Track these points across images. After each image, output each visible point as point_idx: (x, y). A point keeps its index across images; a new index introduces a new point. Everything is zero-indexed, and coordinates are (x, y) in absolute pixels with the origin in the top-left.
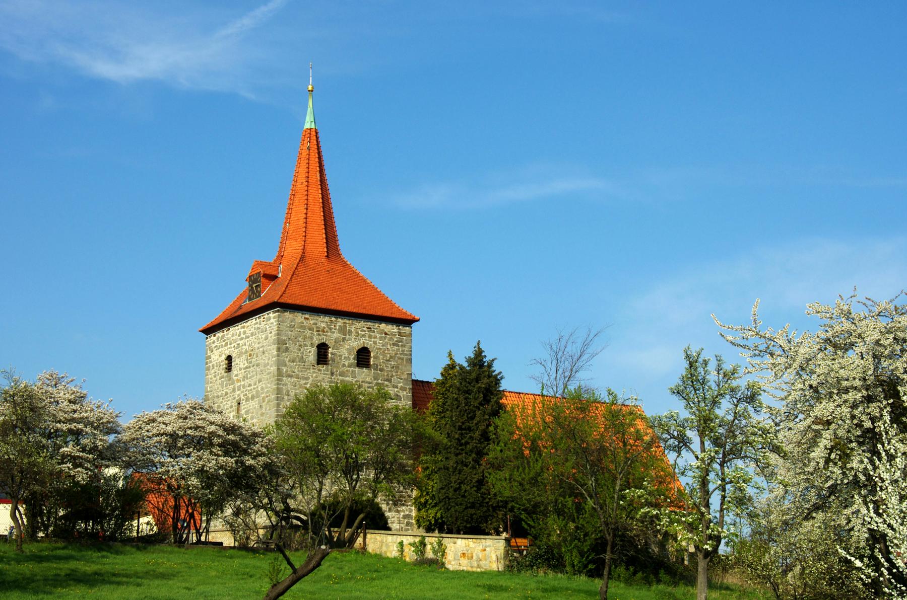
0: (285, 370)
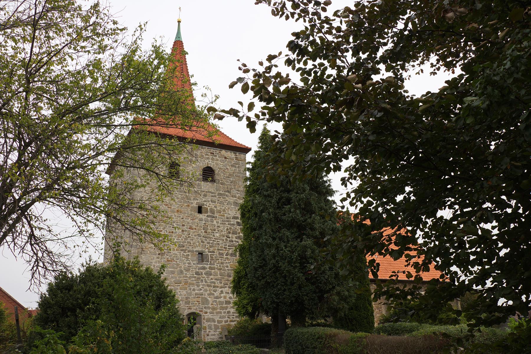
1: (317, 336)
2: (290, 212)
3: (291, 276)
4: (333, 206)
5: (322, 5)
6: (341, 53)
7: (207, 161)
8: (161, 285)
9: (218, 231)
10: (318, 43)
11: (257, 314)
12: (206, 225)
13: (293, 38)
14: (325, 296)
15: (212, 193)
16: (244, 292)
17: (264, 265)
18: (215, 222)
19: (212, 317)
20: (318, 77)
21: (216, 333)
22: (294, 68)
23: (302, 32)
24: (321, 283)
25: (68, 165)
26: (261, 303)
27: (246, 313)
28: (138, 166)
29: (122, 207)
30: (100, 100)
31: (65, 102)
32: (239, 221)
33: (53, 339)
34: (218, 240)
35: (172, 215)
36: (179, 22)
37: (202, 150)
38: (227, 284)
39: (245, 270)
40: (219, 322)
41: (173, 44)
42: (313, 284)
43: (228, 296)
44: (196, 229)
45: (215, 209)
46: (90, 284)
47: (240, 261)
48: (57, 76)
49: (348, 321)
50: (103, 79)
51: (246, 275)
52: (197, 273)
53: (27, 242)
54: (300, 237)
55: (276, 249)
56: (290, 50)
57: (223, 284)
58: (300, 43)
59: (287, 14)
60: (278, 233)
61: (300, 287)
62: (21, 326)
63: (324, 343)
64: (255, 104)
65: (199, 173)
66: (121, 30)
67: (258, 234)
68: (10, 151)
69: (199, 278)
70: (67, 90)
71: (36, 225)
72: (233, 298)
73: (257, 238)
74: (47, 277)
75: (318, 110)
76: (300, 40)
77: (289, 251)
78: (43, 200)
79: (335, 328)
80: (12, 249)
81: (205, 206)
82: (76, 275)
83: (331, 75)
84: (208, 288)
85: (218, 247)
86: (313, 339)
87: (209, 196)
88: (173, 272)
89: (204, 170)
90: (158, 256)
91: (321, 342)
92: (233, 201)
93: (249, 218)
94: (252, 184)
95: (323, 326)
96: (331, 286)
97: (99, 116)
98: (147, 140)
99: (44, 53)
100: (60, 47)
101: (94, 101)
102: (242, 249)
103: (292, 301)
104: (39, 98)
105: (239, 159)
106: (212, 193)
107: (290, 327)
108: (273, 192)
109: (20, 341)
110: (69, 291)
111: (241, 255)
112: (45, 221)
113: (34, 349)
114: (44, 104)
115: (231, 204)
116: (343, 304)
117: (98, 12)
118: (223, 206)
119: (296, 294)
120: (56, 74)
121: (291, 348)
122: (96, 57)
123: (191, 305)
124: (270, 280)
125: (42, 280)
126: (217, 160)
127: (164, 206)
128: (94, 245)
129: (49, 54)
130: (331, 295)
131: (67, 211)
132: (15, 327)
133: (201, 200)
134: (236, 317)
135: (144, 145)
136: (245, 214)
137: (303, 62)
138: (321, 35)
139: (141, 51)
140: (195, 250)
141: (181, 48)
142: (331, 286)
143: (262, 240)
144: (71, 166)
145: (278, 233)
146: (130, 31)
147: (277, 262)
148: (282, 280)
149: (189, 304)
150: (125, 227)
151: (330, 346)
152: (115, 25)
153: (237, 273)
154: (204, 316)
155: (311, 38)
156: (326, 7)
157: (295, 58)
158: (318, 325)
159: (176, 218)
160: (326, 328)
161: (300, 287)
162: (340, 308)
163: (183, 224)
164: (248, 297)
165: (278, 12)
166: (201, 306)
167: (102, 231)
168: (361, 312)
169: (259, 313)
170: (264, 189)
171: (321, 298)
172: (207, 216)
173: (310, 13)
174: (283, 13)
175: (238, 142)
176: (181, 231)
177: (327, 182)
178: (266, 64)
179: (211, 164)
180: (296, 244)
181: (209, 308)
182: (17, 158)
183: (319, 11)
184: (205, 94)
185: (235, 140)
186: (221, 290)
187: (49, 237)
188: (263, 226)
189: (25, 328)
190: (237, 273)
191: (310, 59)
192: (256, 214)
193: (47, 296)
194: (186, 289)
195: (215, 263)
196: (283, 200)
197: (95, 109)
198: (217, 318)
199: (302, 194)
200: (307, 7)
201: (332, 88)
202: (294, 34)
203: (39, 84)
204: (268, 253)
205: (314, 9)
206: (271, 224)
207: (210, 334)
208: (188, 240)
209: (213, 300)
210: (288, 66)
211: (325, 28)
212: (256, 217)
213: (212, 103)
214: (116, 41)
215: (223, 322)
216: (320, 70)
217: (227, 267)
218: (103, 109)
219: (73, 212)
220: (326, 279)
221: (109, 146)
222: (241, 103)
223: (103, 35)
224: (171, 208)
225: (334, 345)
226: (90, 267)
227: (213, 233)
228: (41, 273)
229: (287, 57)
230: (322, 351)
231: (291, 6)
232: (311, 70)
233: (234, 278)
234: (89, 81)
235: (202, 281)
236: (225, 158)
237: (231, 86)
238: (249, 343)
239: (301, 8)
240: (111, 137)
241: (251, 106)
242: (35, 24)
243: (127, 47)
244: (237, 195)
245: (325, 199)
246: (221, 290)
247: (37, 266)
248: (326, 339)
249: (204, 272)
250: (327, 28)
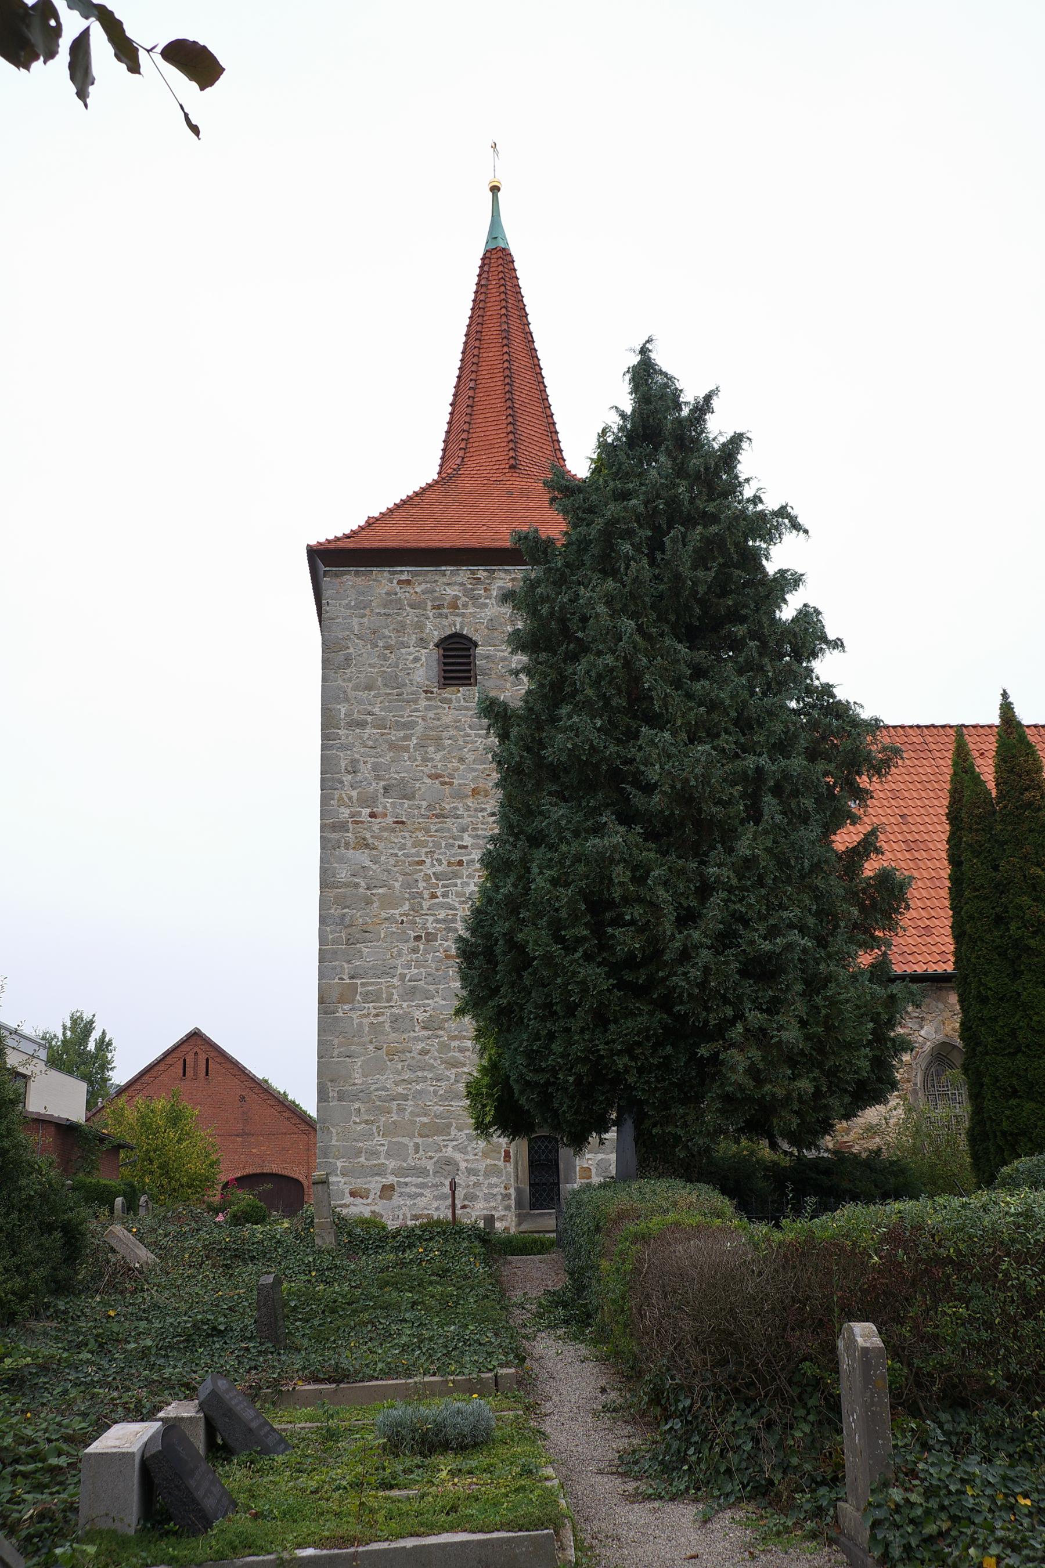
0: (343, 710)
35: (456, 808)
36: (495, 189)
90: (412, 944)
127: (428, 781)
159: (470, 816)
161: (601, 1019)
224: (451, 784)
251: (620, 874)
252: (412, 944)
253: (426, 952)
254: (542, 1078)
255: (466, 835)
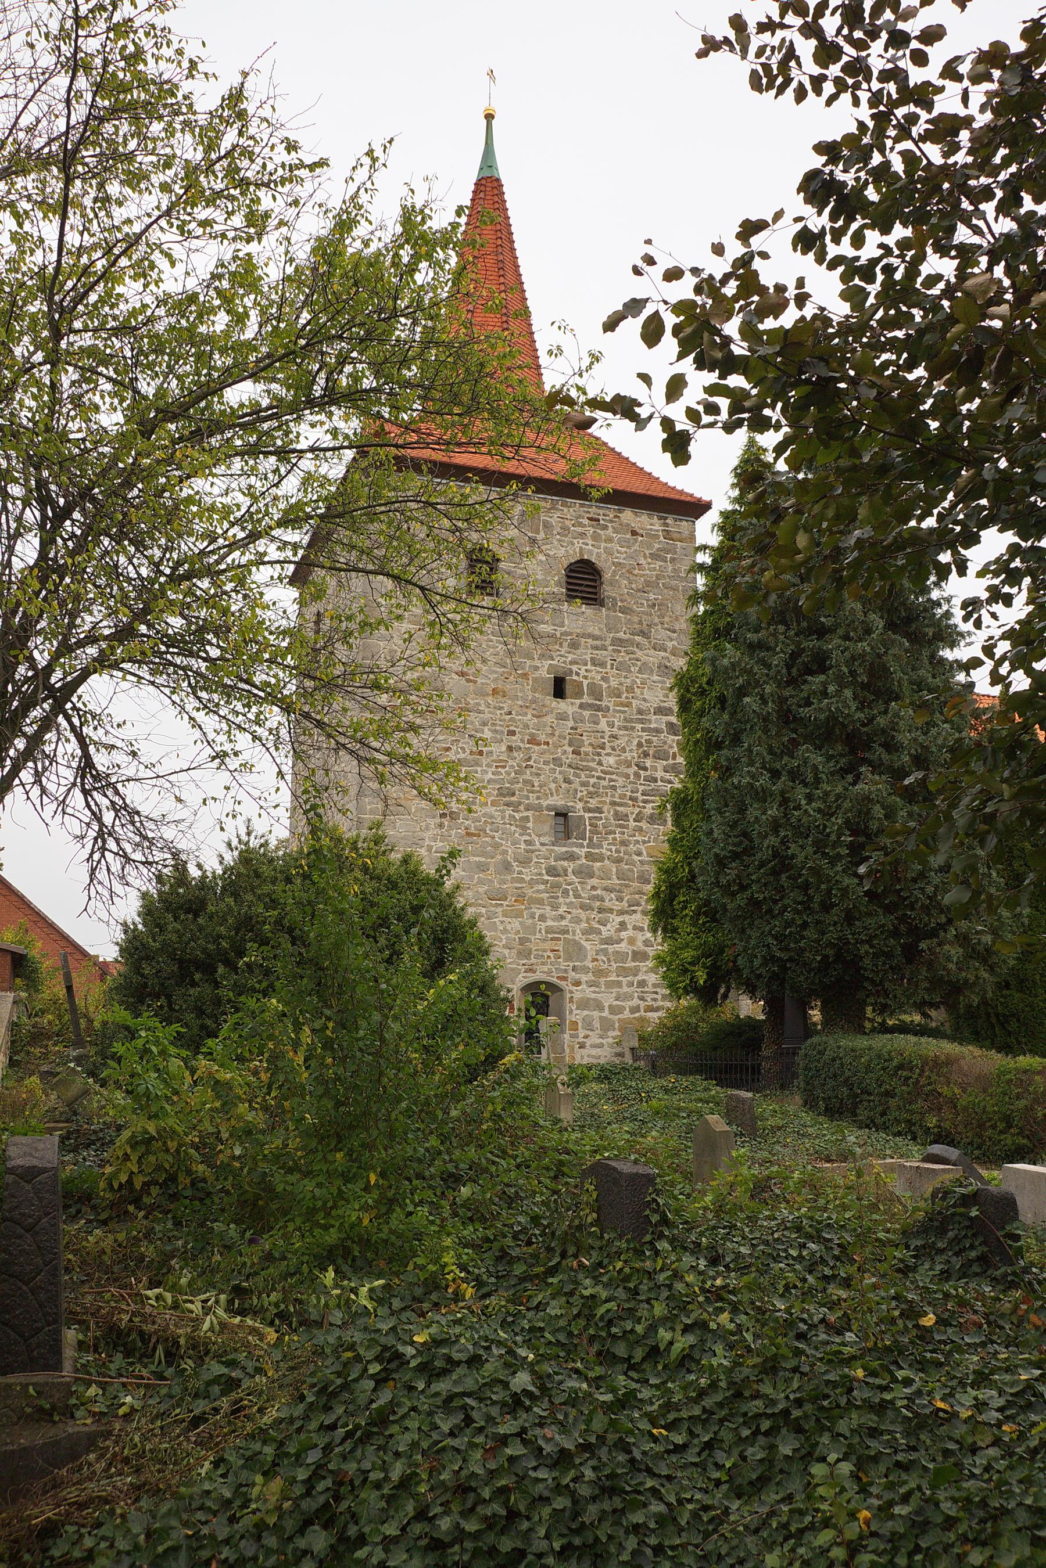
1: (895, 1063)
2: (825, 694)
3: (823, 887)
4: (958, 678)
5: (915, 44)
6: (971, 203)
7: (578, 544)
8: (445, 904)
9: (614, 749)
10: (896, 173)
11: (722, 991)
12: (579, 731)
13: (818, 161)
14: (923, 945)
15: (596, 638)
16: (685, 927)
17: (745, 849)
18: (603, 724)
19: (593, 996)
20: (896, 283)
21: (604, 1041)
22: (820, 259)
23: (848, 138)
24: (913, 909)
25: (174, 569)
26: (735, 962)
27: (693, 989)
28: (370, 567)
29: (330, 686)
30: (254, 376)
31: (160, 388)
32: (673, 719)
33: (157, 1043)
34: (614, 777)
35: (478, 704)
36: (489, 117)
37: (565, 510)
38: (638, 904)
39: (690, 864)
40: (613, 1010)
41: (473, 188)
42: (889, 909)
43: (641, 937)
44: (548, 744)
45: (605, 685)
46: (249, 897)
47: (674, 839)
48: (134, 313)
49: (994, 1020)
50: (262, 313)
51: (693, 878)
52: (552, 871)
53: (74, 784)
54: (851, 771)
55: (780, 806)
56: (807, 201)
57: (625, 904)
58: (840, 176)
59: (800, 82)
60: (786, 759)
61: (849, 918)
62: (79, 1001)
63: (918, 1081)
64: (687, 378)
65: (555, 584)
66: (312, 167)
67: (728, 760)
68: (18, 535)
69: (558, 886)
70: (163, 353)
71: (96, 738)
72: (657, 945)
73: (726, 772)
74: (129, 879)
75: (879, 394)
76: (841, 167)
77: (819, 810)
78: (110, 667)
79: (952, 1039)
80: (37, 803)
81: (575, 677)
82: (214, 873)
83: (939, 277)
84: (583, 915)
85: (613, 796)
86: (884, 1069)
87: (587, 648)
88: (482, 868)
89: (571, 571)
90: (438, 820)
91: (907, 1079)
92: (656, 661)
93: (701, 713)
94: (712, 612)
95: (916, 1035)
96: (943, 916)
97: (252, 423)
98: (394, 490)
99: (94, 247)
100: (137, 228)
101: (235, 383)
102: (681, 804)
103: (825, 957)
104: (88, 376)
105: (675, 536)
106: (596, 638)
107: (817, 1032)
108: (774, 635)
109: (79, 1043)
110: (196, 915)
111: (677, 822)
112: (119, 726)
113: (112, 1063)
114: (102, 397)
115: (652, 671)
116: (977, 969)
117: (242, 115)
118: (626, 677)
119: (839, 939)
120: (130, 306)
121: (818, 1092)
122: (239, 250)
123: (533, 961)
124: (762, 897)
125: (118, 888)
126: (610, 540)
127: (456, 677)
128: (256, 794)
129: (108, 251)
130: (940, 945)
131: (175, 697)
132: (66, 1006)
133: (562, 659)
134: (664, 997)
135: (385, 505)
136: (690, 701)
137: (852, 238)
138: (908, 145)
139: (371, 223)
140: (545, 803)
141: (496, 199)
142: (943, 916)
143: (741, 779)
144: (181, 571)
145: (786, 759)
146: (338, 170)
147: (782, 843)
148: (796, 895)
149: (528, 956)
150: (338, 743)
151: (935, 1090)
152: (293, 153)
153: (666, 872)
154: (571, 992)
155: (877, 159)
156: (927, 49)
157: (823, 228)
158: (904, 1029)
160: (923, 1040)
161: (849, 918)
162: (966, 981)
163: (512, 728)
164: (697, 942)
165: (772, 80)
166: (563, 964)
167: (274, 754)
168: (1036, 996)
169: (728, 990)
170: (747, 624)
171: (911, 953)
172: (582, 706)
173: (875, 74)
174: (788, 81)
175: (671, 484)
176: (504, 748)
177: (939, 605)
178: (735, 250)
179: (590, 552)
180: (839, 789)
181: (585, 970)
182: (35, 555)
183: (901, 64)
184: (559, 348)
185: (663, 479)
186: (620, 919)
187: (130, 772)
188: (744, 737)
189: (92, 1009)
190: (666, 872)
191: (872, 227)
192: (722, 700)
193: (140, 927)
194: (519, 915)
195: (605, 845)
196: (804, 658)
197: (242, 405)
198: (608, 999)
199: (861, 640)
200: (864, 54)
201: (940, 316)
202: (821, 148)
203: (87, 340)
204: (756, 818)
205: (888, 61)
206: (765, 731)
207: (588, 1043)
208: (525, 777)
209: (599, 947)
210: (804, 252)
211: (922, 121)
212: (723, 709)
213: (581, 375)
214: (296, 203)
215: (627, 1012)
216: (903, 261)
217: (639, 854)
218: (265, 402)
219: (191, 703)
220: (929, 897)
221: (286, 512)
222: (645, 378)
223: (257, 186)
224: (475, 682)
225: (945, 1090)
226: (248, 851)
227: (599, 754)
228: (113, 869)
229: (800, 226)
230: (910, 1103)
231: (814, 55)
232: (873, 262)
233: (658, 887)
234: (221, 321)
235: (566, 893)
236: (634, 533)
237: (611, 325)
238: (699, 1072)
239: (845, 59)
240: (291, 486)
241: (676, 387)
242: (67, 161)
243: (330, 215)
244: (670, 645)
245: (933, 655)
246: (620, 919)
247: (103, 849)
248: (923, 1071)
249: (571, 866)
250: (927, 122)
251: (878, 811)
252: (438, 820)
253: (450, 828)
254: (784, 956)
255: (486, 729)
